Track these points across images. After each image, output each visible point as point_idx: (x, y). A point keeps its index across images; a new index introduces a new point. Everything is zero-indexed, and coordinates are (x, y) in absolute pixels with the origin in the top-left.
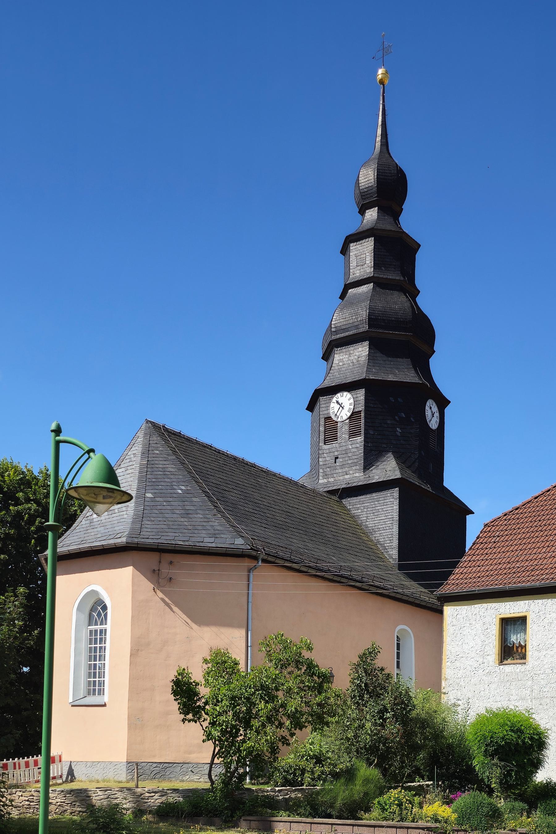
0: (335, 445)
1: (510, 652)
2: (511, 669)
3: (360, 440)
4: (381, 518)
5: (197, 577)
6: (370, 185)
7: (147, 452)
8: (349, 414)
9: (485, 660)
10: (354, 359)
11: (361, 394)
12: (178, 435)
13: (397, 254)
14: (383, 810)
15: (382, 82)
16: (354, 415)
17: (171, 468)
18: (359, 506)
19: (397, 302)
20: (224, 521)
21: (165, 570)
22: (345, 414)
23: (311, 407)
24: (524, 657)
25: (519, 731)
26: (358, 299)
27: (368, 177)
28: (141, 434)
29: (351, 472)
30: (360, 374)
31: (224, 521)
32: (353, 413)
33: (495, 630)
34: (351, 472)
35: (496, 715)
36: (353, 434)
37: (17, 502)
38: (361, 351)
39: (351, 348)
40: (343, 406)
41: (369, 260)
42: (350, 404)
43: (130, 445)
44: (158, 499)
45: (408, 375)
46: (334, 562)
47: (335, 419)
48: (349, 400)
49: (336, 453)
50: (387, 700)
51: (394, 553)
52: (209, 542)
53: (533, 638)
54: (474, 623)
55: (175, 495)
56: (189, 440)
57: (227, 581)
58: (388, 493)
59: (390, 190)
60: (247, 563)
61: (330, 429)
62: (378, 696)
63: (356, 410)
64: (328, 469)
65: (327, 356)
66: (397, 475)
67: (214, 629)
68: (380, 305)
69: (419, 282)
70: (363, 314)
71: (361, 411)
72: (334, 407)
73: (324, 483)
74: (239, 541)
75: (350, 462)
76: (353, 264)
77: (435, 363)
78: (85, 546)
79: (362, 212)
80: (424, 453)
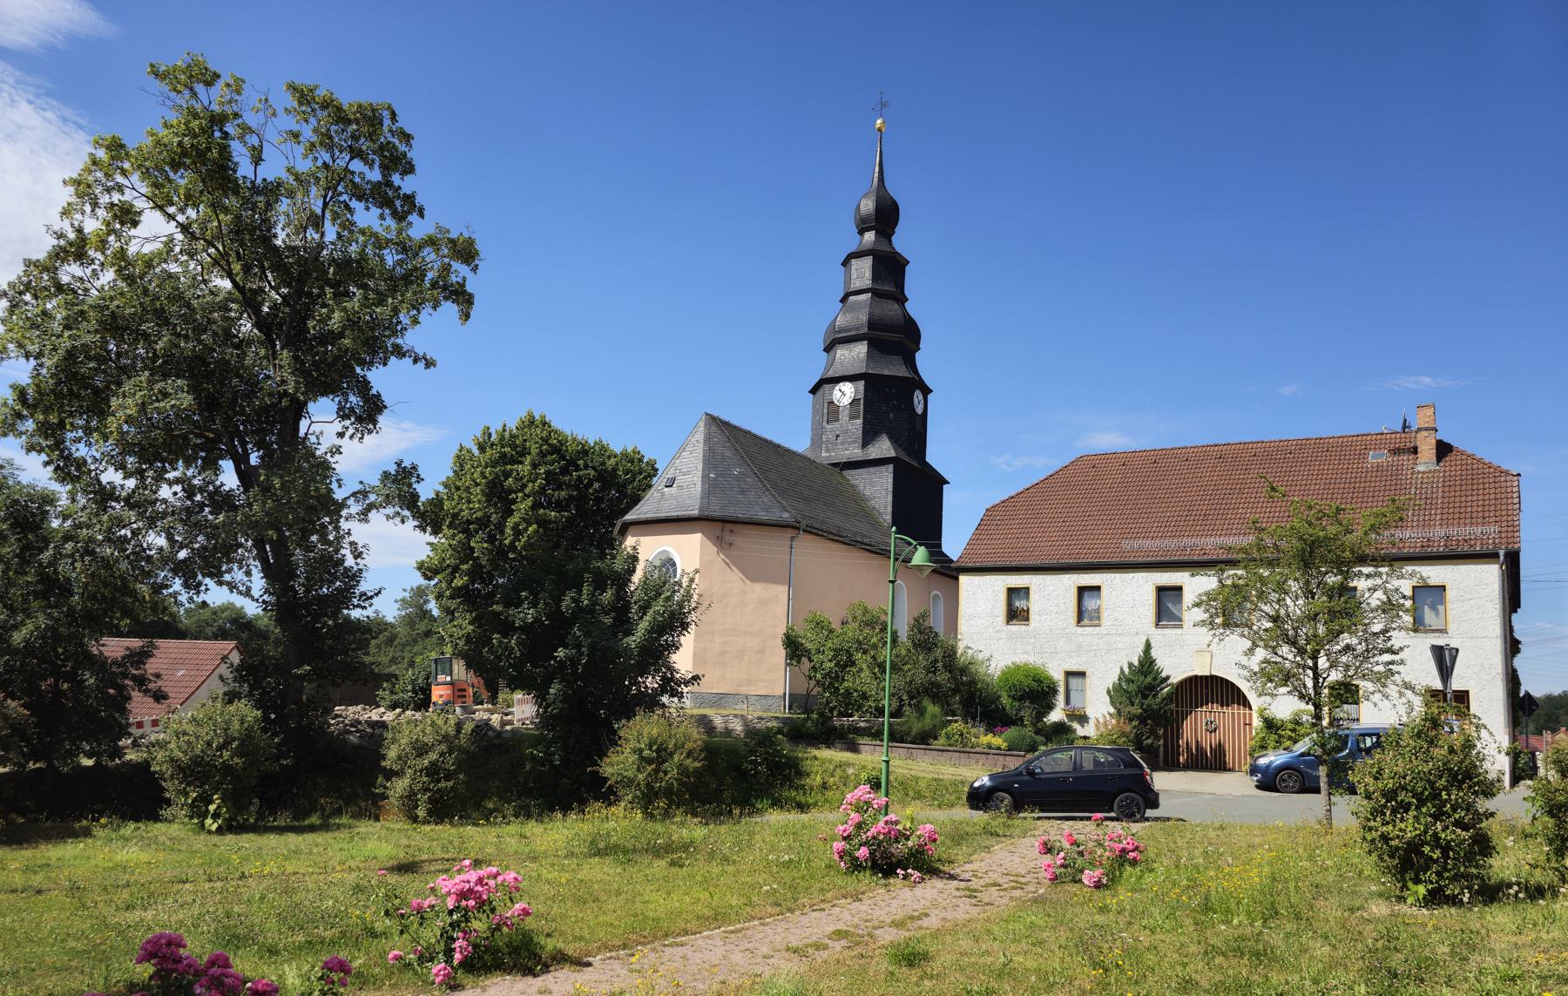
0: (837, 425)
1: (1016, 614)
2: (1016, 628)
3: (859, 422)
4: (878, 489)
5: (752, 543)
7: (708, 439)
10: (854, 355)
11: (861, 384)
12: (726, 424)
13: (890, 269)
14: (948, 738)
16: (854, 402)
17: (728, 453)
18: (858, 478)
19: (890, 309)
20: (762, 495)
21: (728, 537)
22: (846, 401)
23: (814, 391)
24: (1027, 619)
25: (1039, 681)
26: (858, 306)
27: (868, 206)
28: (702, 424)
30: (861, 368)
31: (762, 495)
33: (1003, 596)
35: (1018, 667)
36: (853, 417)
37: (577, 469)
38: (861, 349)
39: (852, 345)
40: (845, 394)
41: (868, 274)
43: (693, 433)
45: (899, 370)
46: (835, 521)
50: (938, 653)
51: (889, 518)
52: (763, 516)
53: (1036, 604)
56: (735, 427)
57: (773, 547)
58: (884, 468)
60: (790, 533)
61: (833, 411)
62: (930, 650)
65: (828, 349)
66: (892, 454)
67: (764, 585)
68: (877, 312)
70: (863, 318)
72: (836, 394)
73: (825, 456)
74: (786, 515)
76: (854, 276)
77: (921, 358)
78: (662, 515)
79: (861, 232)
80: (912, 434)
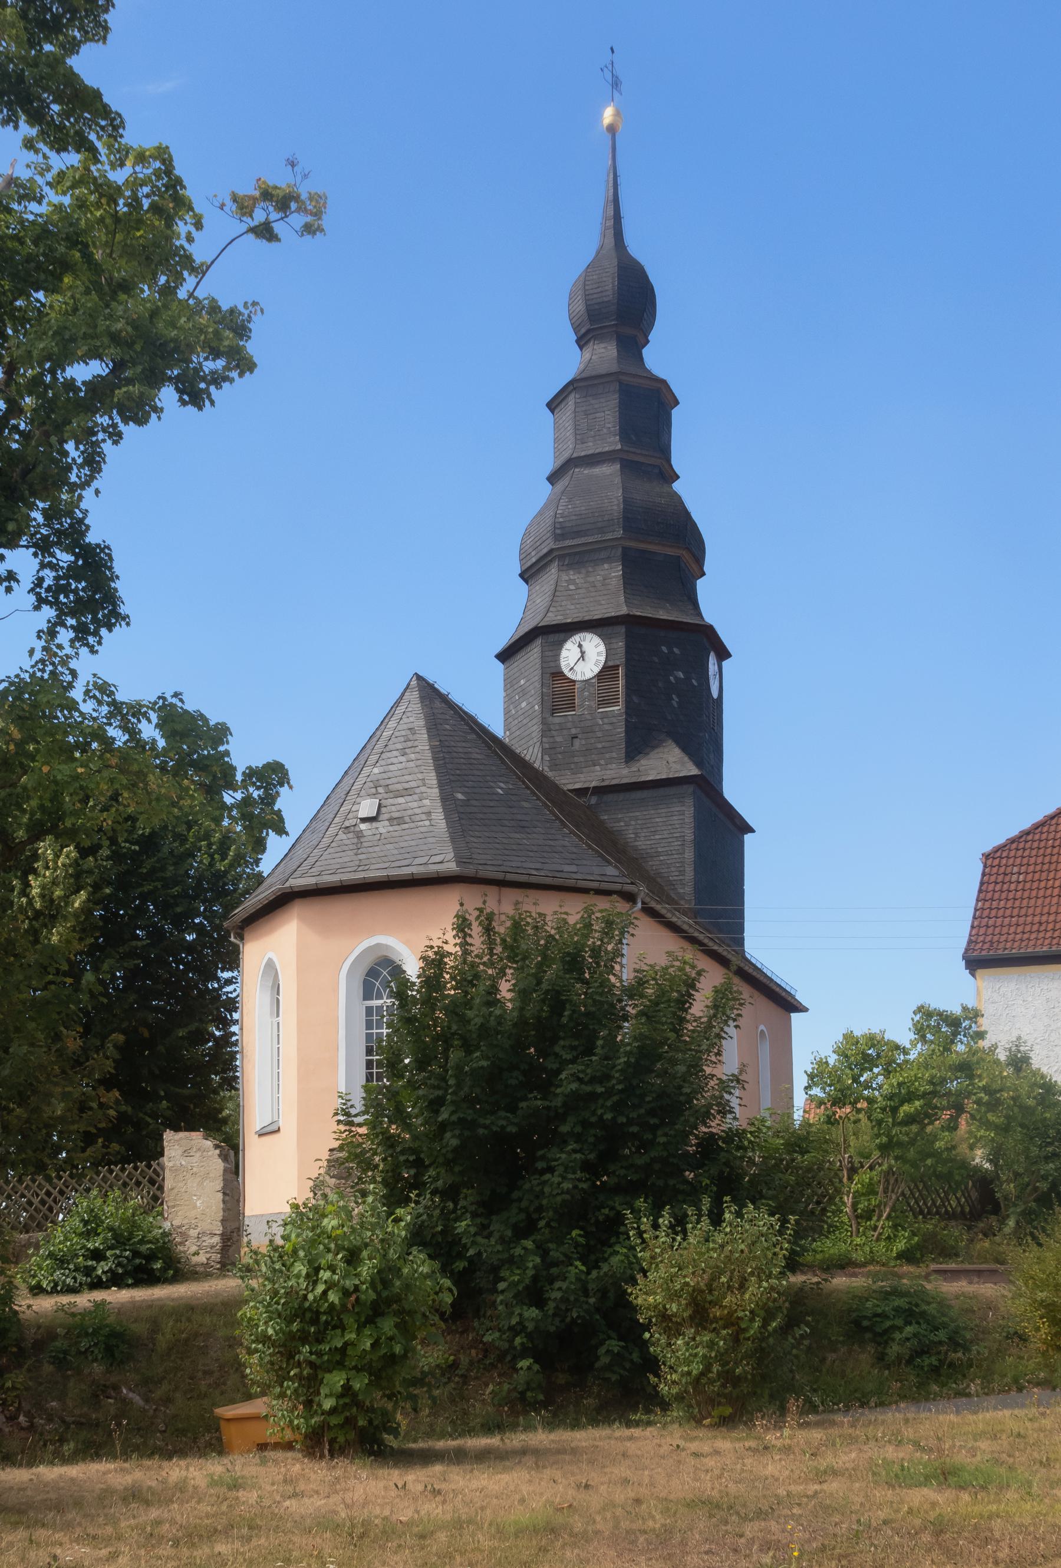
6: (606, 299)
8: (597, 670)
9: (1051, 1053)
12: (444, 699)
13: (642, 414)
15: (612, 129)
16: (607, 672)
29: (602, 762)
32: (603, 668)
34: (602, 762)
42: (599, 654)
44: (474, 802)
47: (569, 675)
48: (596, 646)
49: (573, 731)
54: (1030, 999)
55: (495, 797)
59: (621, 307)
63: (610, 664)
64: (560, 756)
69: (677, 462)
71: (618, 666)
75: (600, 746)
